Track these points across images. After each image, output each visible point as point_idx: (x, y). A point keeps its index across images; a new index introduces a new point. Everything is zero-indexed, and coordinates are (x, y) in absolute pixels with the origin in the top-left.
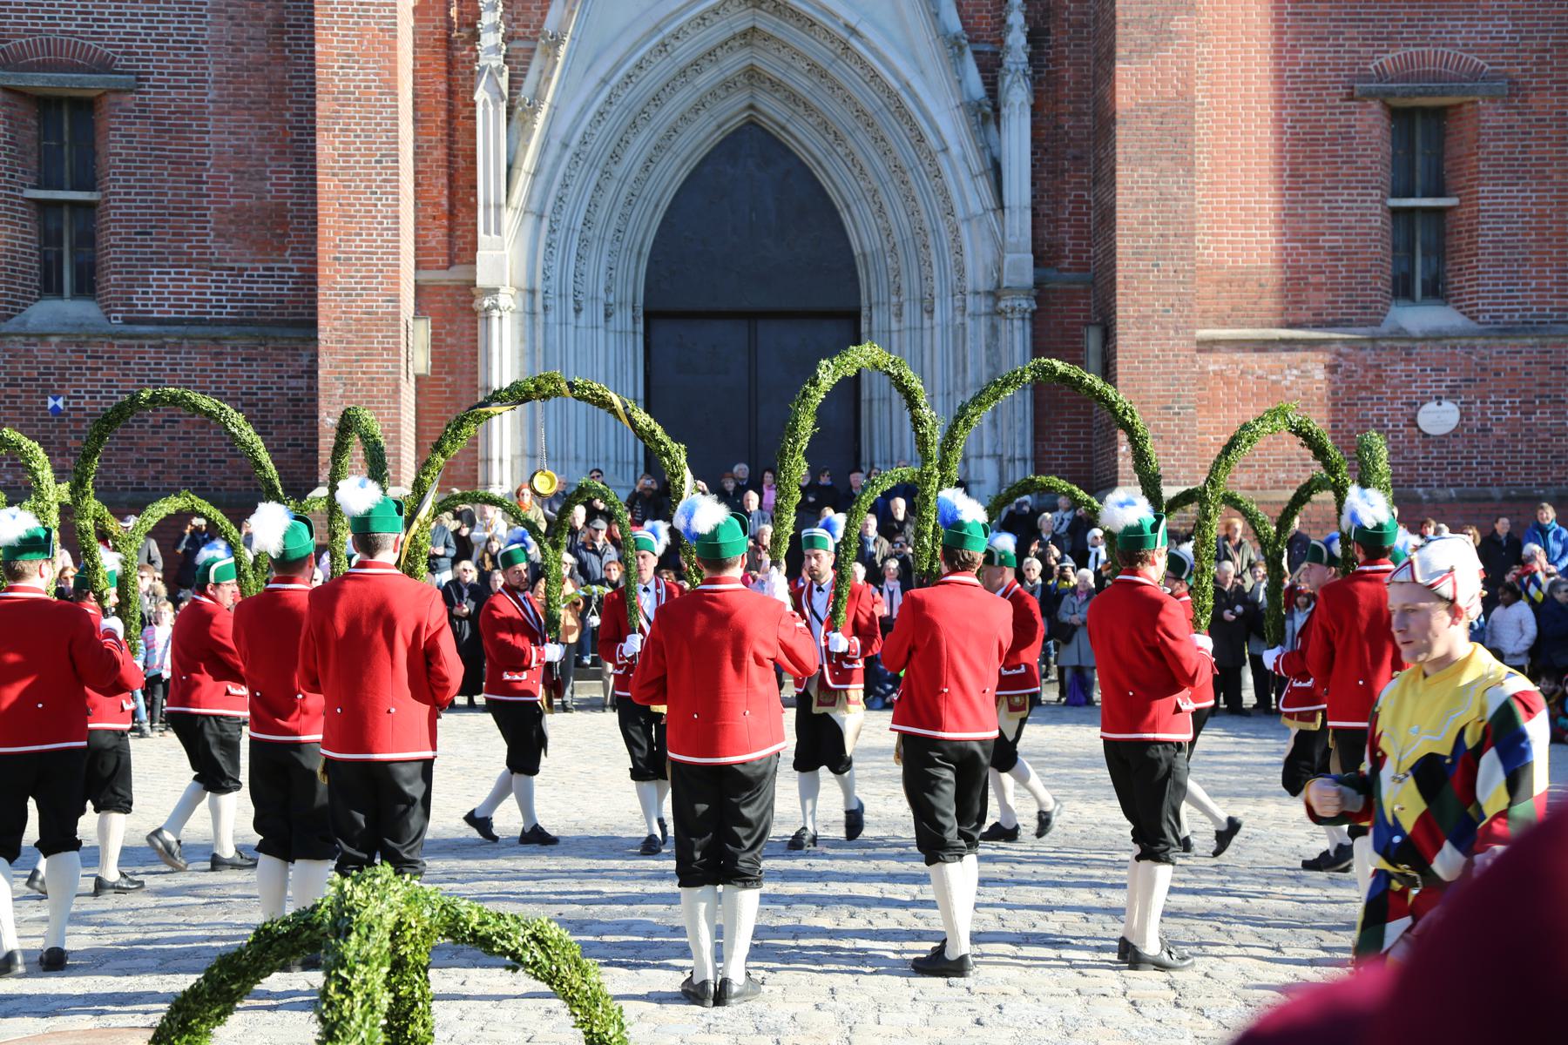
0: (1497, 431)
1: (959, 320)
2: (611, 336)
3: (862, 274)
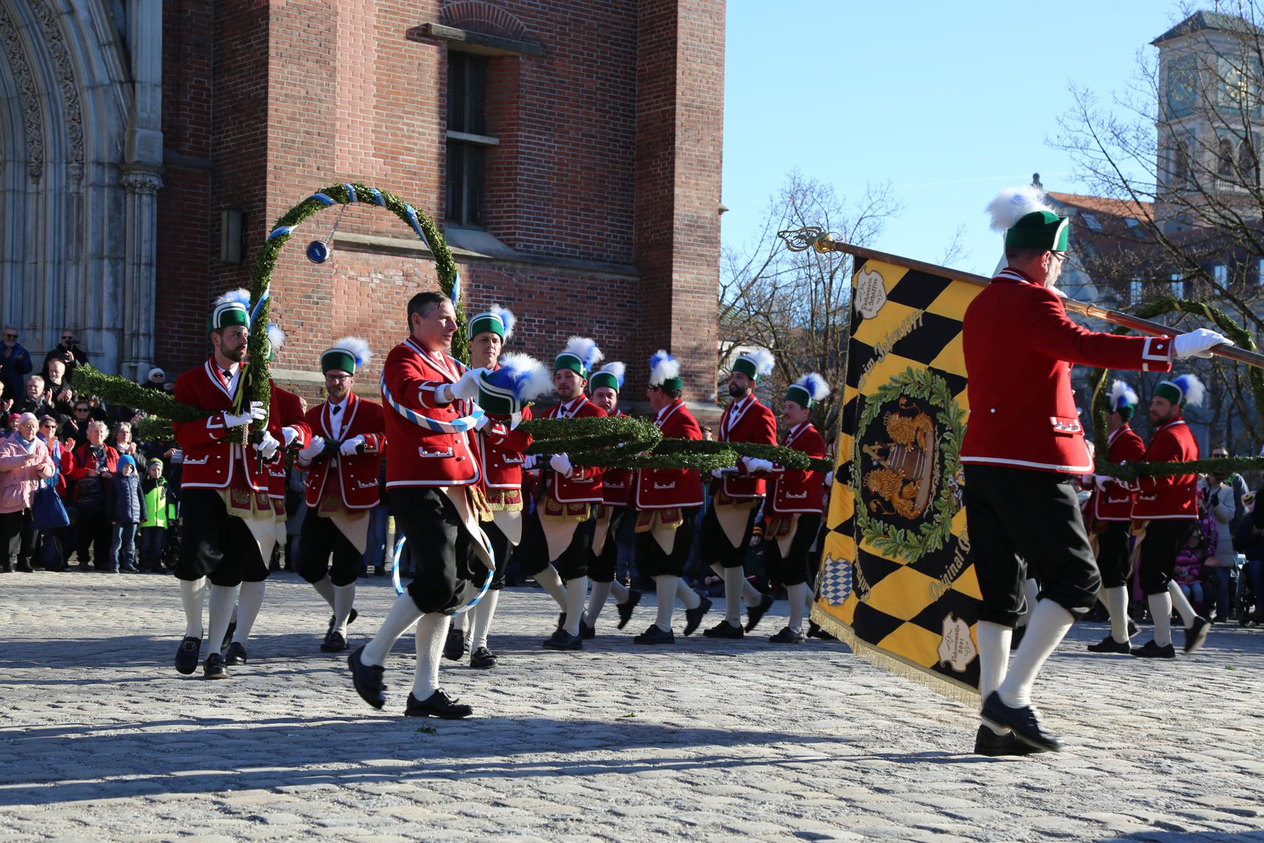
1: (73, 188)
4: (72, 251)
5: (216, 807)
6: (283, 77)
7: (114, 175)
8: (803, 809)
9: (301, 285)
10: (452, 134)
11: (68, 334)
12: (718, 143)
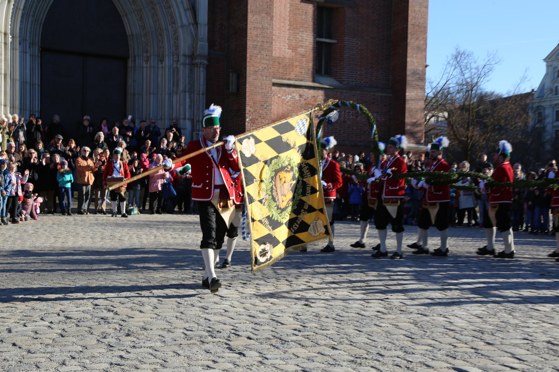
0: (349, 122)
1: (175, 65)
4: (175, 89)
5: (227, 346)
6: (253, 21)
8: (457, 354)
10: (318, 39)
11: (174, 121)
12: (425, 39)
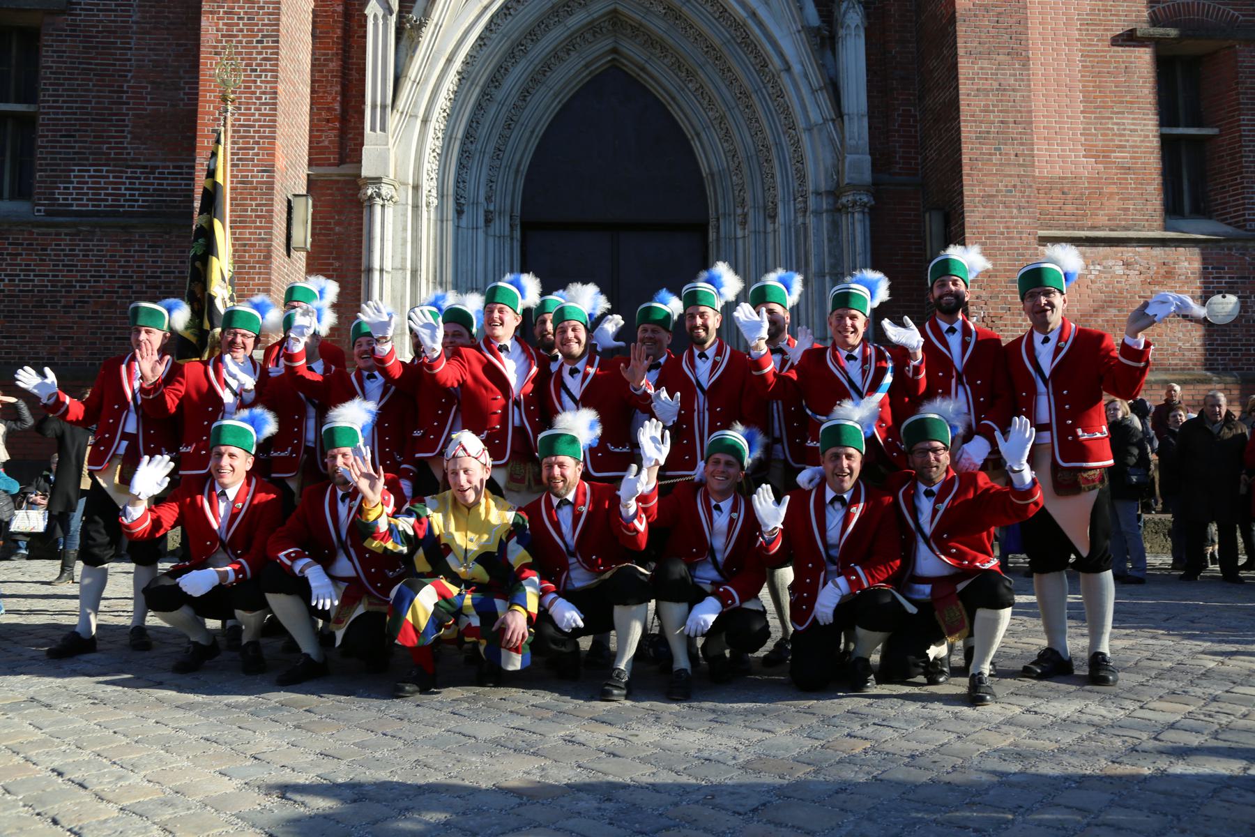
1: (800, 220)
2: (491, 240)
3: (710, 192)
6: (973, 75)
7: (831, 201)
9: (1005, 271)
